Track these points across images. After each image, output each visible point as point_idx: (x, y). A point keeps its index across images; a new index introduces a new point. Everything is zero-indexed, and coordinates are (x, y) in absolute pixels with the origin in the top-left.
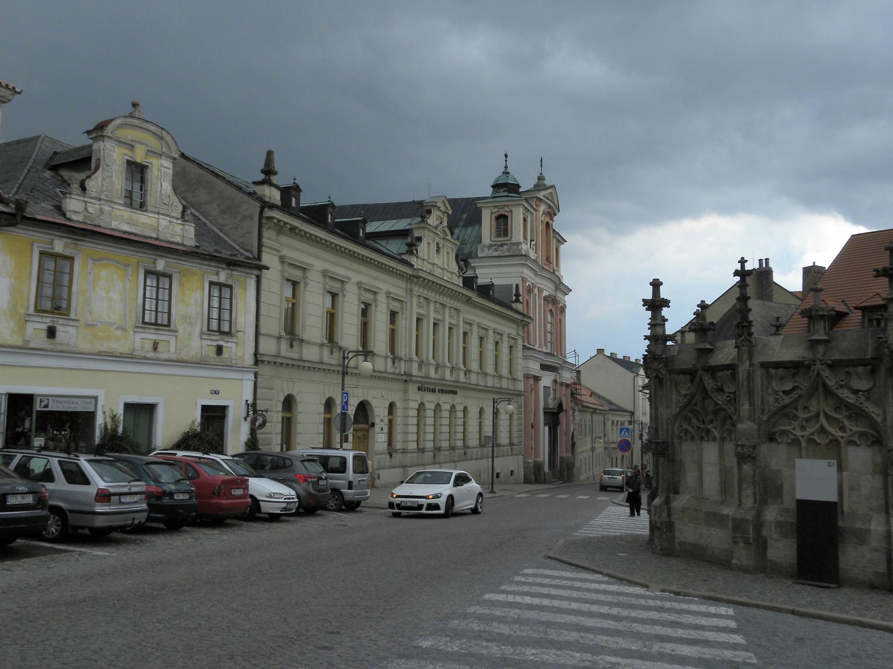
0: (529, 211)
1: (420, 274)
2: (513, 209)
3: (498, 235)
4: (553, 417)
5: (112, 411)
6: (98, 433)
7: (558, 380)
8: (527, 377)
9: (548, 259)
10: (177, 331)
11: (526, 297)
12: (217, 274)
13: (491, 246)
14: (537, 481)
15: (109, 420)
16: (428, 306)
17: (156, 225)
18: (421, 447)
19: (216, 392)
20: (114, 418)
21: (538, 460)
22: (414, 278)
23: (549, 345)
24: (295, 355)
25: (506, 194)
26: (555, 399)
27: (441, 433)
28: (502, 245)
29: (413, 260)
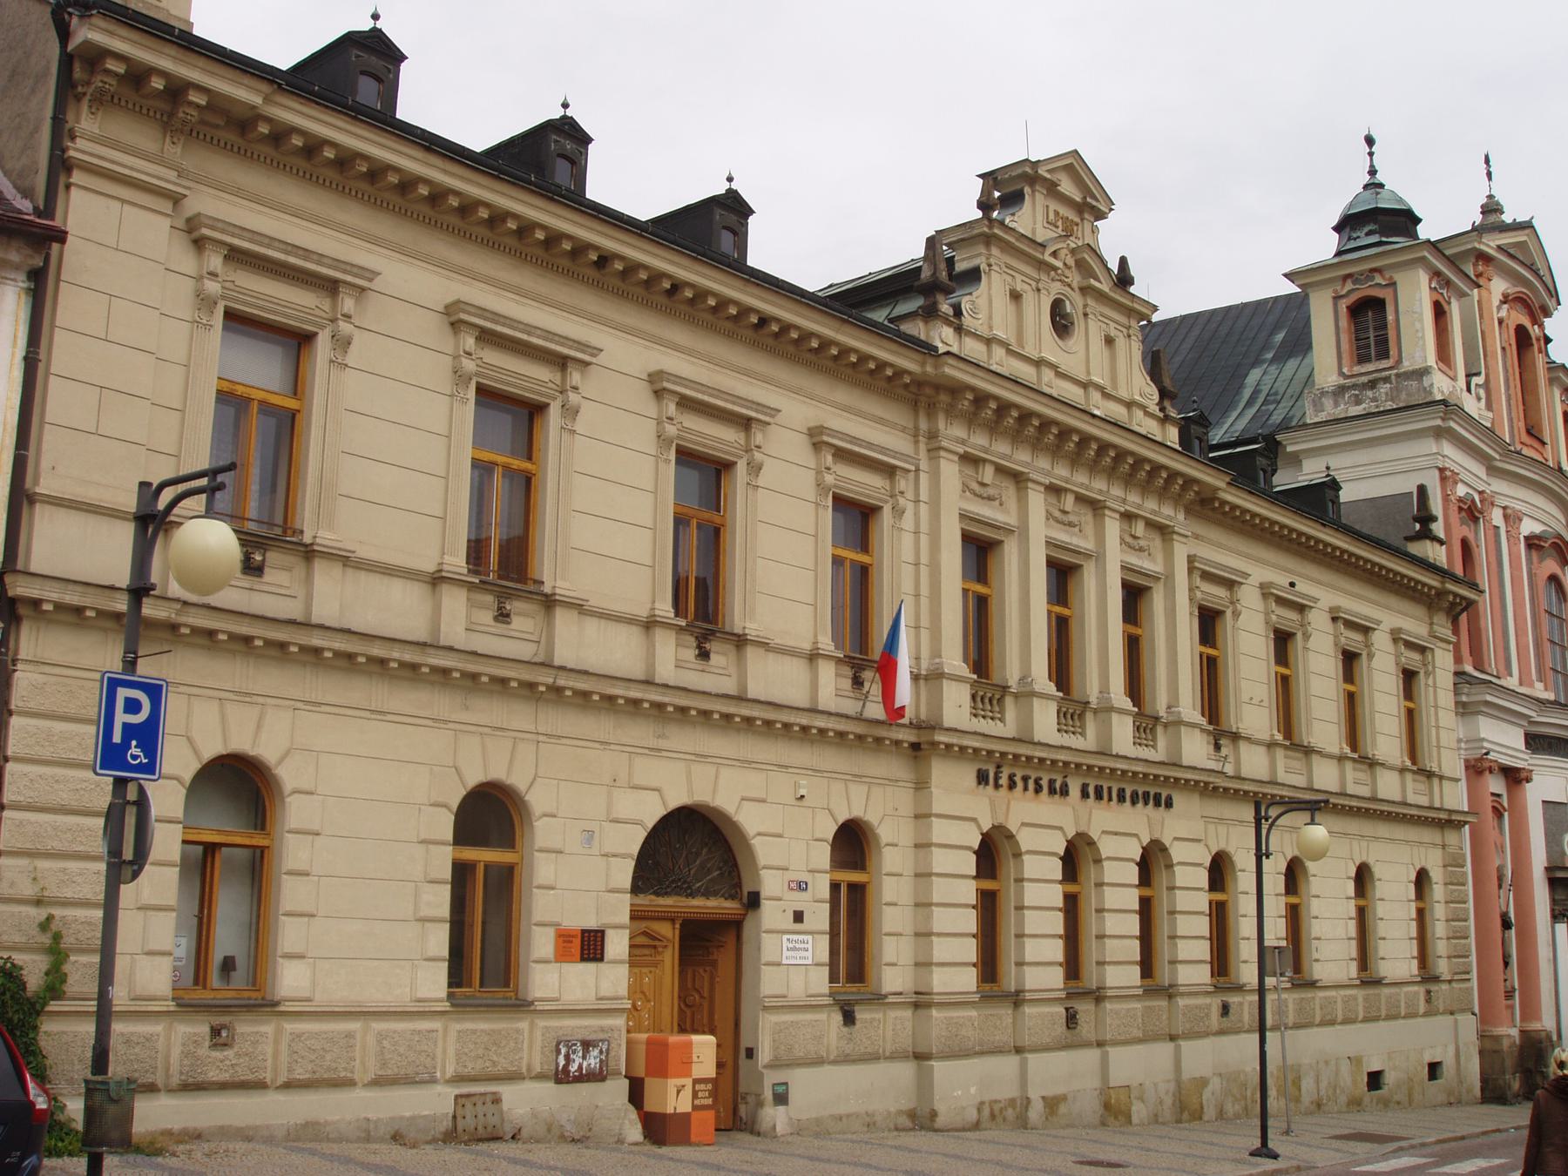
3: (1362, 359)
9: (1533, 432)
11: (1461, 530)
13: (1340, 391)
24: (1159, 754)
25: (1375, 239)
28: (1372, 385)
29: (943, 337)
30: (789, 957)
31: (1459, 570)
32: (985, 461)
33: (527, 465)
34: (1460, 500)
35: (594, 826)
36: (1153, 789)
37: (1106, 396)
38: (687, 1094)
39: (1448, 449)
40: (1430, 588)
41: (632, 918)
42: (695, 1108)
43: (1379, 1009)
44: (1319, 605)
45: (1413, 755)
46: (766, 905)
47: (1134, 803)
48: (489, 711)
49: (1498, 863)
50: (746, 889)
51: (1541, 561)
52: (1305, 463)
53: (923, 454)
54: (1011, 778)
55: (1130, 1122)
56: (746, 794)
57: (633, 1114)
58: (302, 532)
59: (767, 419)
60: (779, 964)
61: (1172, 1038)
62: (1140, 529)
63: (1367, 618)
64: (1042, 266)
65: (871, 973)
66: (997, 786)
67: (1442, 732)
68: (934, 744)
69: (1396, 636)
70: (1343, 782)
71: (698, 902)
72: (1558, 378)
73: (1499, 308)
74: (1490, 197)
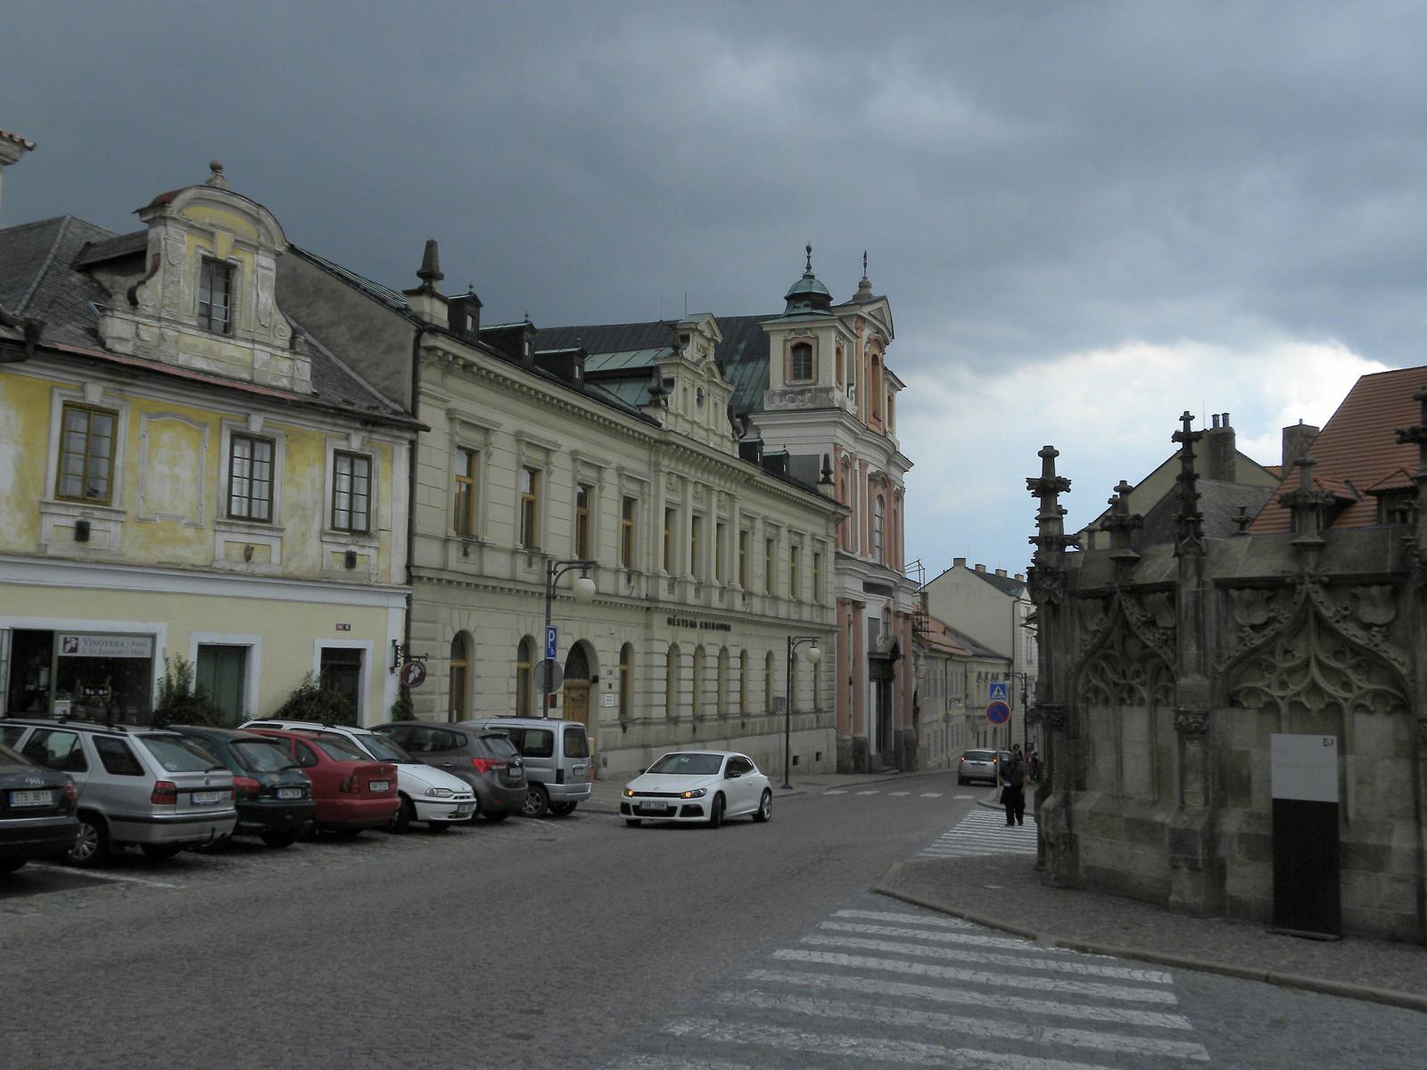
1: (672, 438)
2: (821, 334)
3: (797, 376)
5: (179, 658)
6: (156, 693)
7: (892, 607)
8: (842, 602)
9: (876, 415)
10: (282, 530)
12: (347, 438)
13: (784, 393)
14: (858, 770)
15: (174, 672)
16: (684, 490)
17: (249, 360)
19: (345, 628)
20: (182, 668)
22: (661, 445)
23: (877, 551)
25: (808, 310)
26: (887, 638)
28: (802, 393)
29: (660, 416)
31: (840, 501)
37: (715, 434)
44: (562, 449)
45: (768, 588)
46: (601, 682)
50: (591, 675)
51: (875, 487)
53: (652, 474)
68: (657, 608)
69: (813, 537)
72: (888, 379)
74: (865, 278)
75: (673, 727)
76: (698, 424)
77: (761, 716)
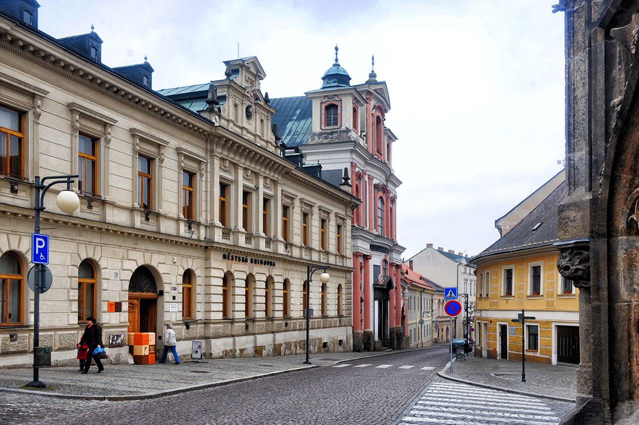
0: (358, 101)
3: (328, 124)
4: (383, 293)
7: (388, 260)
8: (356, 255)
11: (356, 182)
13: (320, 135)
14: (367, 349)
18: (271, 315)
21: (368, 330)
23: (380, 228)
24: (252, 246)
25: (336, 84)
27: (255, 303)
28: (332, 133)
29: (214, 119)
30: (171, 310)
31: (355, 195)
32: (226, 159)
33: (93, 158)
34: (357, 173)
35: (118, 272)
36: (269, 261)
37: (261, 139)
38: (148, 349)
39: (354, 156)
40: (347, 200)
41: (129, 299)
42: (150, 353)
43: (327, 325)
46: (165, 295)
47: (265, 264)
48: (86, 237)
49: (360, 283)
50: (158, 291)
51: (378, 192)
52: (307, 157)
54: (232, 256)
55: (262, 356)
56: (160, 262)
57: (131, 356)
58: (28, 179)
59: (166, 145)
60: (169, 312)
61: (273, 332)
62: (268, 181)
63: (329, 210)
64: (244, 95)
65: (193, 315)
66: (229, 259)
67: (347, 244)
69: (336, 215)
70: (320, 259)
71: (145, 294)
72: (387, 133)
73: (372, 110)
74: (373, 71)
75: (229, 325)
76: (246, 129)
77: (300, 319)
